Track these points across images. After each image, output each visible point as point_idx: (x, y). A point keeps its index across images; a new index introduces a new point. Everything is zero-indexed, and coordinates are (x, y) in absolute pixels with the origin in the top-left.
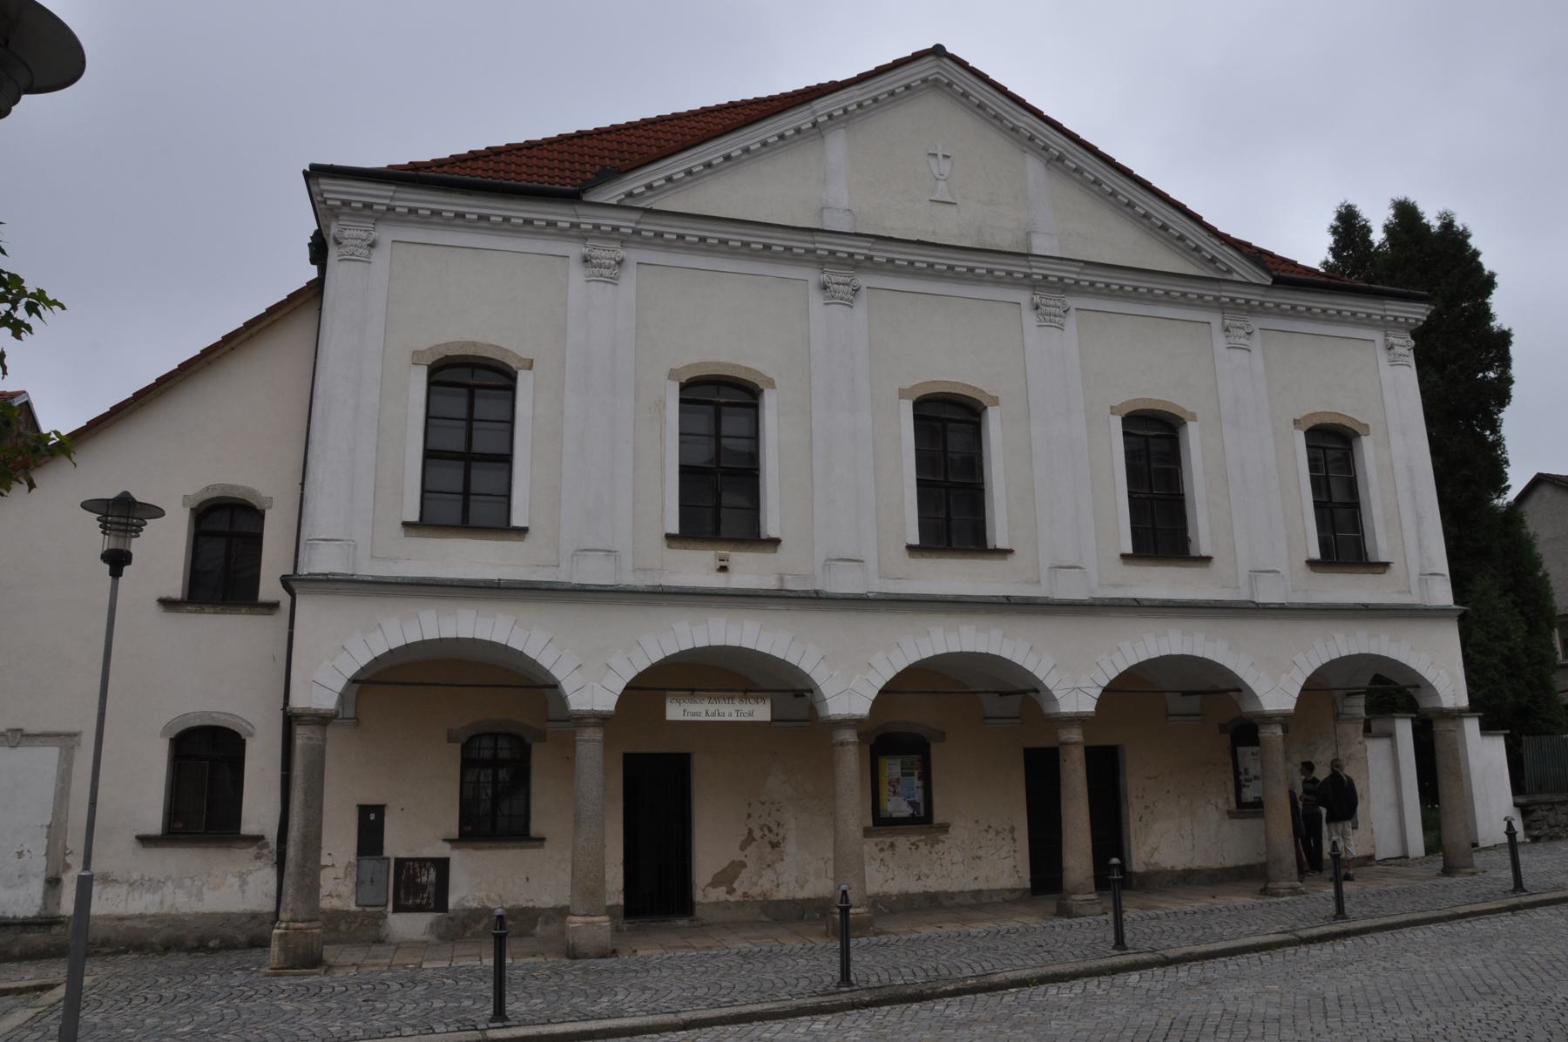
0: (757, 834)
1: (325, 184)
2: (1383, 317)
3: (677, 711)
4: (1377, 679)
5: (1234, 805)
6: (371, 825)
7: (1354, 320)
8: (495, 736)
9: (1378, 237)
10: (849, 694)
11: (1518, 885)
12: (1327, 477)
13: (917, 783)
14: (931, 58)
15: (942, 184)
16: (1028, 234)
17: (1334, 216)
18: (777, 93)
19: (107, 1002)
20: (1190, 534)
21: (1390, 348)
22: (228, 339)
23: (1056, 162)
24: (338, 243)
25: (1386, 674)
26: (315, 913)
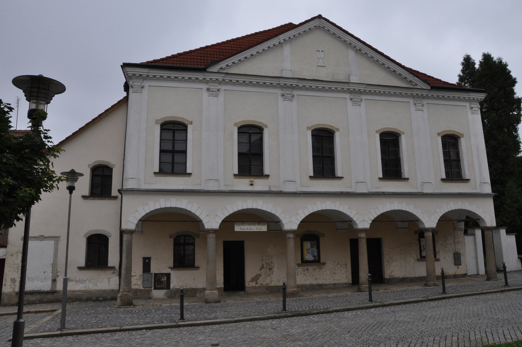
0: (265, 266)
1: (128, 69)
2: (469, 98)
3: (238, 228)
4: (467, 217)
5: (419, 257)
6: (147, 264)
7: (459, 99)
8: (185, 236)
9: (477, 66)
10: (291, 222)
11: (507, 284)
12: (449, 151)
13: (315, 250)
14: (317, 19)
15: (321, 60)
16: (349, 75)
17: (463, 59)
18: (271, 28)
19: (72, 315)
20: (402, 171)
21: (472, 108)
22: (100, 116)
23: (358, 51)
24: (132, 87)
25: (469, 215)
26: (130, 290)
